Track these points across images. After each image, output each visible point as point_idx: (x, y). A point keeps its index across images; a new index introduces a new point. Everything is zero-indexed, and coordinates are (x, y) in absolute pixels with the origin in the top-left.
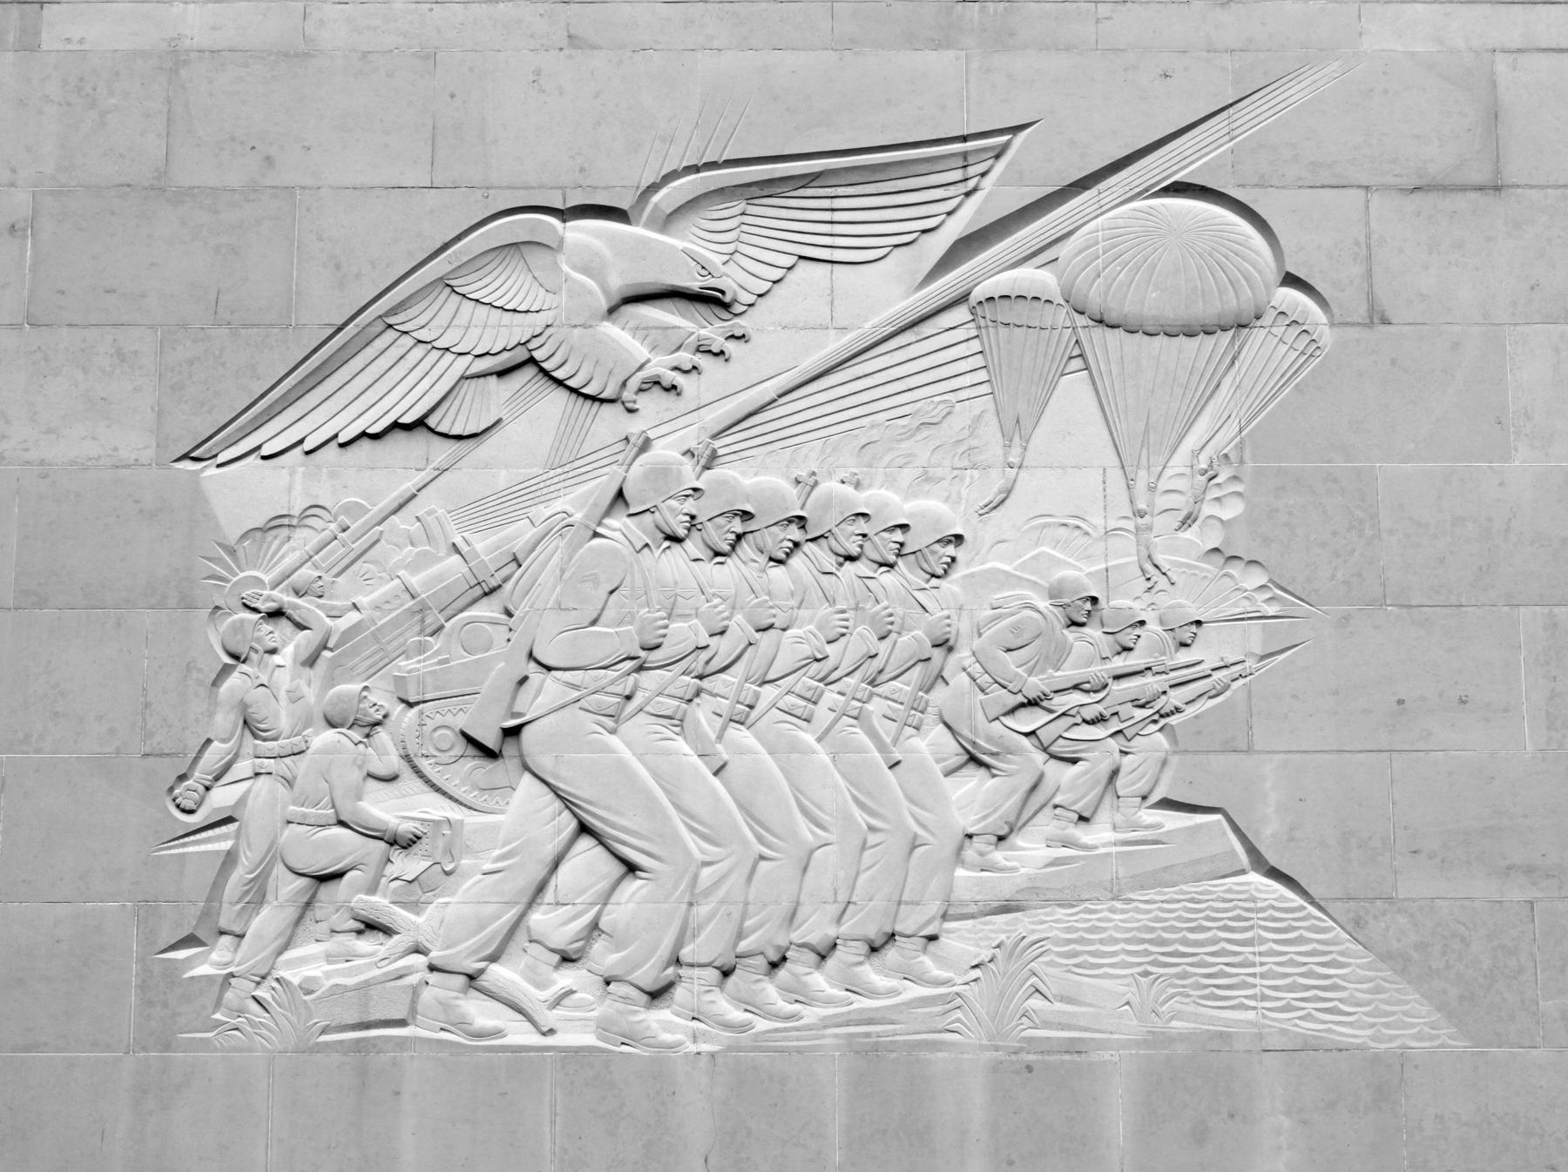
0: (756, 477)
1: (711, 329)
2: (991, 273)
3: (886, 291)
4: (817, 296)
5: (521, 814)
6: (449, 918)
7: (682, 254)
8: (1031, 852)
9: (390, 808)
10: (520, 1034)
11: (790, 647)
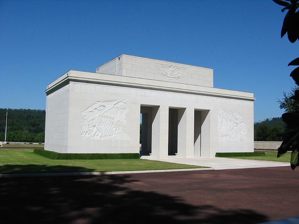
0: (105, 114)
5: (95, 129)
6: (93, 134)
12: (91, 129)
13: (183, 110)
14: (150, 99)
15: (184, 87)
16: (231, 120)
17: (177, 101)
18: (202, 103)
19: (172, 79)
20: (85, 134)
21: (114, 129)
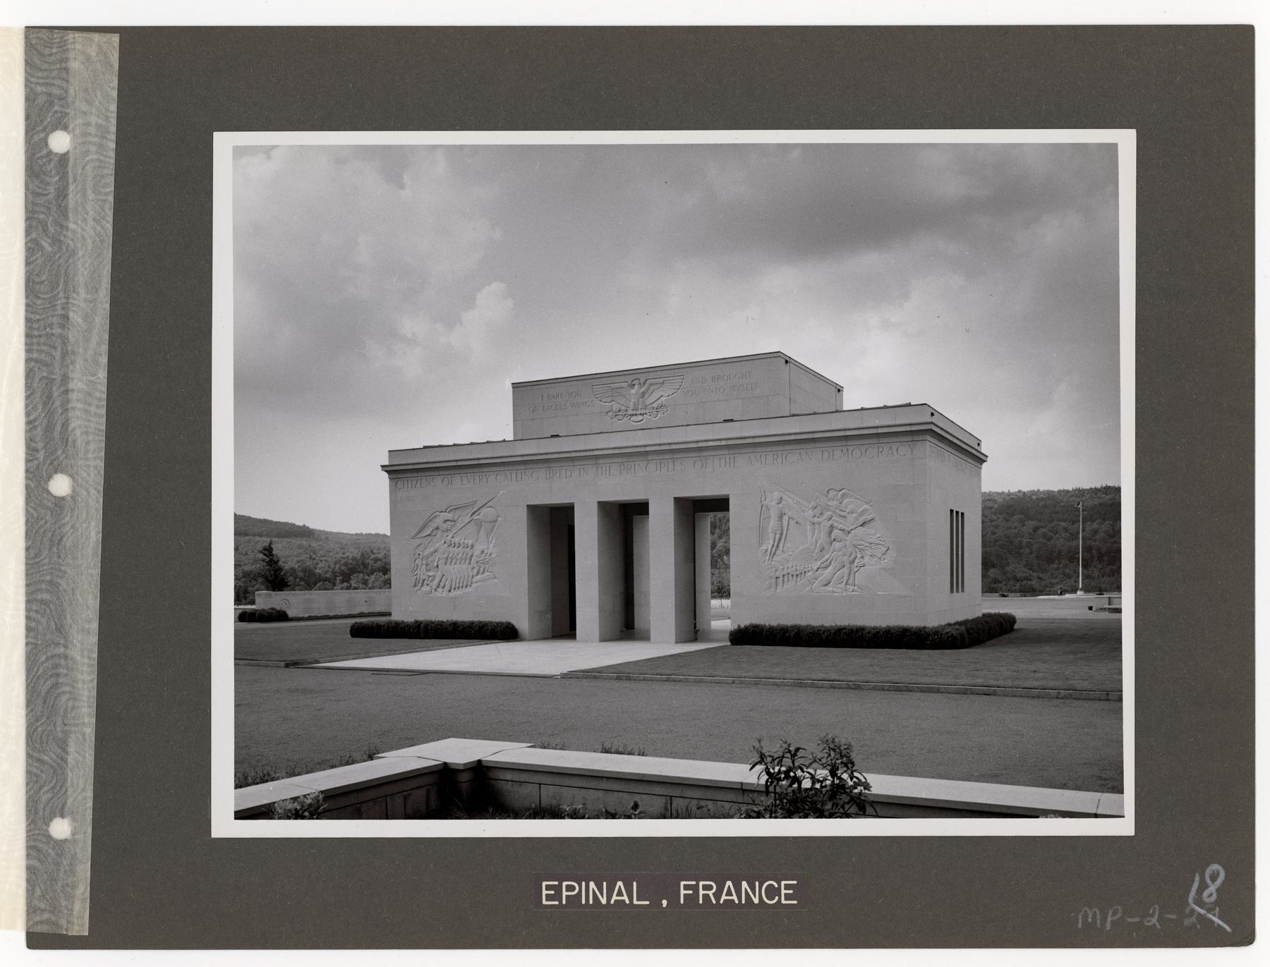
2: (475, 517)
3: (467, 519)
7: (450, 516)
12: (431, 574)
14: (551, 491)
16: (816, 520)
19: (640, 418)
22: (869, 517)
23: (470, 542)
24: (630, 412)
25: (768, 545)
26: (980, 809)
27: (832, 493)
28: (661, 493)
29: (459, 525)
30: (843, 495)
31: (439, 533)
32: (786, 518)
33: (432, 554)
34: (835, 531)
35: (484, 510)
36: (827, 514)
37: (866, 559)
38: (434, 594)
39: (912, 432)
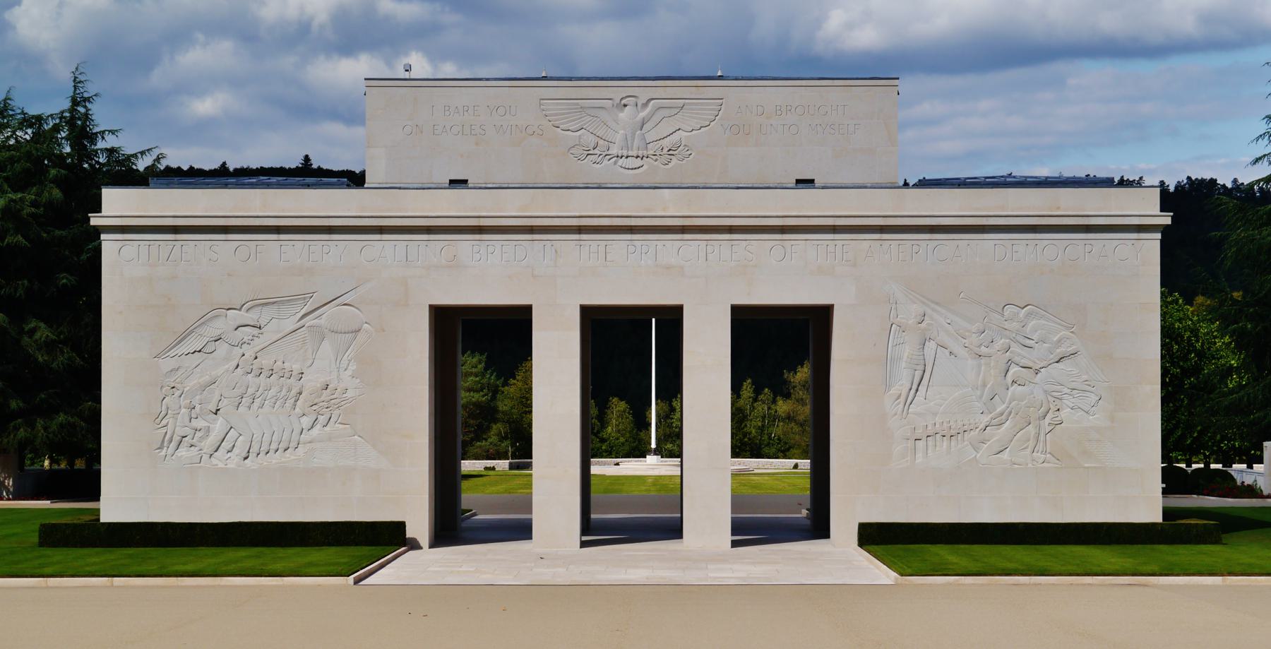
0: (265, 361)
1: (256, 331)
2: (309, 321)
3: (290, 324)
4: (281, 322)
5: (219, 426)
7: (250, 318)
8: (315, 431)
9: (195, 423)
10: (221, 465)
11: (272, 392)
13: (671, 319)
14: (483, 278)
15: (669, 206)
16: (983, 350)
17: (629, 278)
18: (782, 280)
19: (638, 162)
20: (173, 445)
21: (306, 422)
22: (1071, 349)
23: (296, 367)
24: (615, 150)
25: (902, 384)
26: (208, 555)
27: (1009, 310)
28: (706, 297)
29: (268, 335)
30: (1029, 314)
31: (222, 348)
32: (931, 346)
33: (204, 387)
34: (1014, 369)
35: (330, 310)
36: (1001, 343)
37: (1065, 413)
38: (179, 453)
39: (570, 79)
